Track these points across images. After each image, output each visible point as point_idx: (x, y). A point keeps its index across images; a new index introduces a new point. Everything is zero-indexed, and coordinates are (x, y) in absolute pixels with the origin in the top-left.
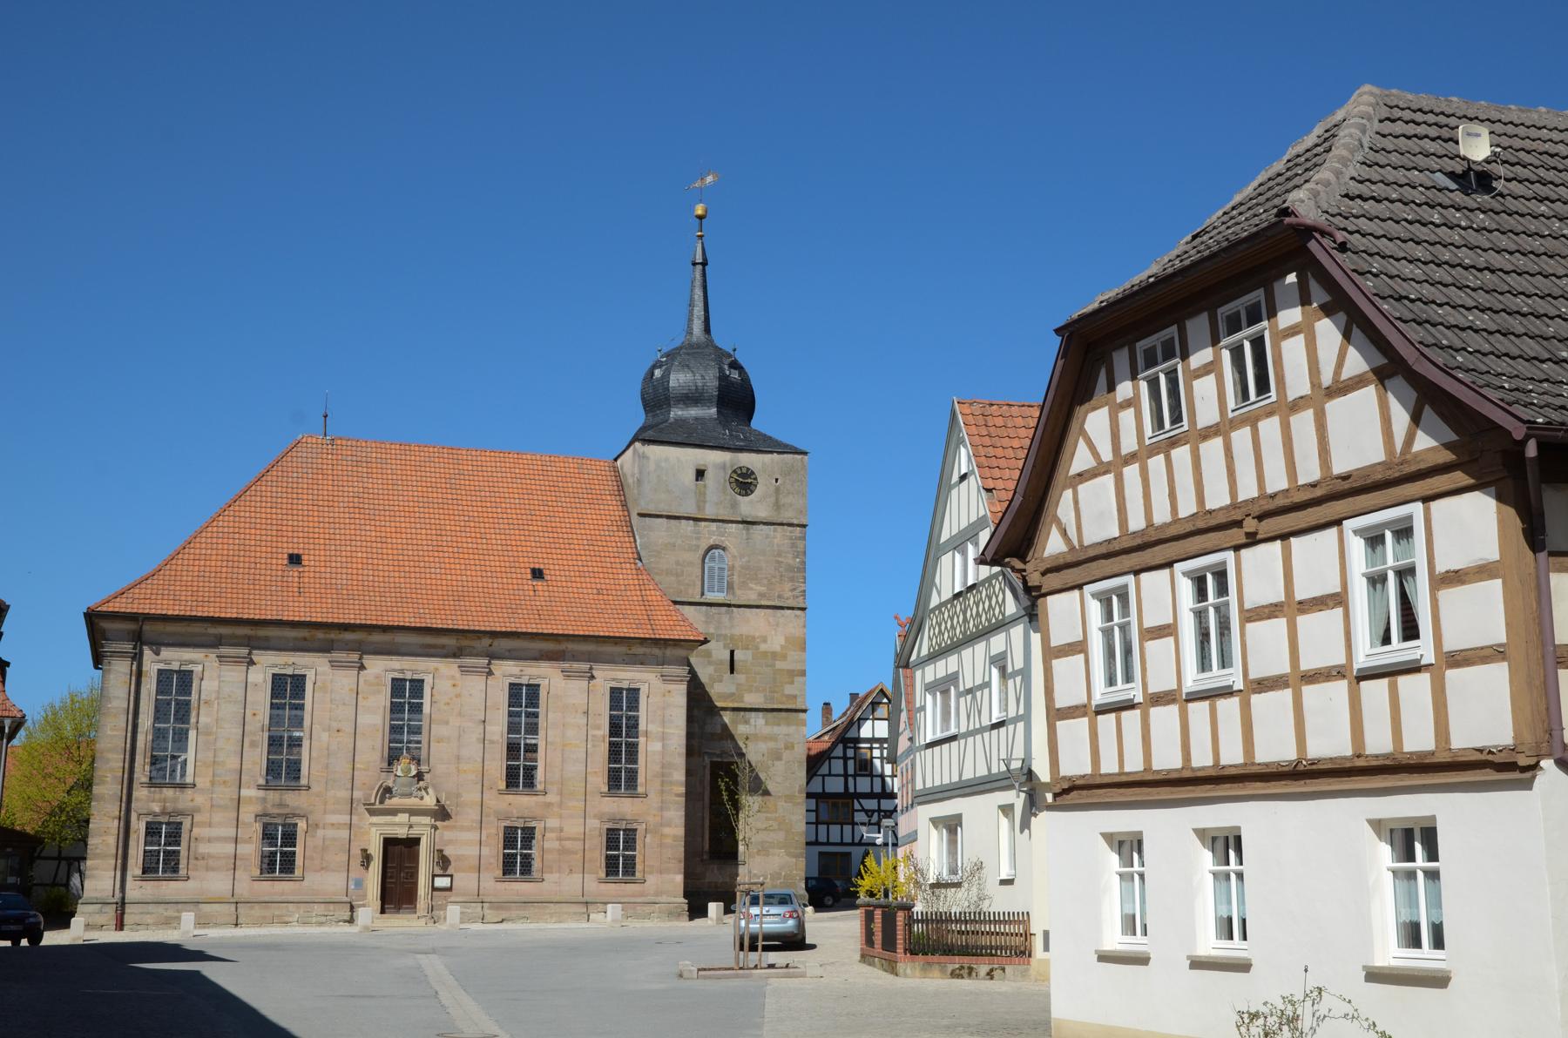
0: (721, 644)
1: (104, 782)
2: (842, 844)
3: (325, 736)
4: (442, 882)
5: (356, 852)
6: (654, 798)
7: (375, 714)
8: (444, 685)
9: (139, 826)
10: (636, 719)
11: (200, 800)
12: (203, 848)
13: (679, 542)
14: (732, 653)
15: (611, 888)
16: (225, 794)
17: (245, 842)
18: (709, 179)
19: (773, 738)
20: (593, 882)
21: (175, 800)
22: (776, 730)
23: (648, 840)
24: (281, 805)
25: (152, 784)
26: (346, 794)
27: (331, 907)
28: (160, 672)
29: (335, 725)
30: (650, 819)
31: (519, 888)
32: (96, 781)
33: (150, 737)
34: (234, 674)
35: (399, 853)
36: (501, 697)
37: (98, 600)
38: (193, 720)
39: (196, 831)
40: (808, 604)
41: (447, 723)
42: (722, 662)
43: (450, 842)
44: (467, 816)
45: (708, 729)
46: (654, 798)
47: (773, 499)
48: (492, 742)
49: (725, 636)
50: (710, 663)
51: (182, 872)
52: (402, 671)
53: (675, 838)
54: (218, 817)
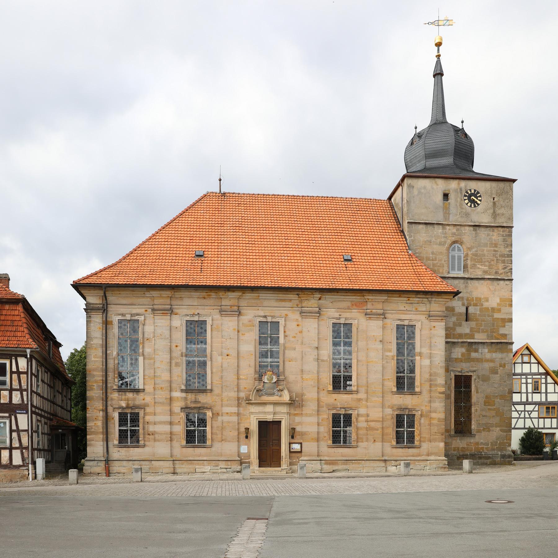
0: (460, 303)
1: (92, 389)
2: (551, 428)
3: (219, 358)
4: (296, 447)
5: (243, 430)
6: (425, 394)
7: (249, 345)
8: (292, 325)
11: (149, 399)
12: (151, 428)
13: (433, 240)
14: (467, 309)
15: (400, 452)
16: (162, 395)
19: (492, 361)
20: (389, 448)
21: (134, 399)
22: (494, 355)
23: (422, 421)
24: (196, 402)
25: (120, 390)
26: (233, 394)
27: (229, 463)
29: (225, 352)
30: (423, 408)
31: (341, 452)
32: (88, 388)
34: (162, 322)
35: (268, 431)
36: (328, 333)
37: (80, 277)
38: (141, 351)
39: (147, 418)
40: (513, 277)
41: (295, 349)
42: (460, 314)
43: (300, 423)
44: (311, 407)
46: (425, 395)
47: (492, 211)
48: (323, 361)
50: (453, 315)
51: (141, 443)
53: (439, 420)
54: (159, 409)
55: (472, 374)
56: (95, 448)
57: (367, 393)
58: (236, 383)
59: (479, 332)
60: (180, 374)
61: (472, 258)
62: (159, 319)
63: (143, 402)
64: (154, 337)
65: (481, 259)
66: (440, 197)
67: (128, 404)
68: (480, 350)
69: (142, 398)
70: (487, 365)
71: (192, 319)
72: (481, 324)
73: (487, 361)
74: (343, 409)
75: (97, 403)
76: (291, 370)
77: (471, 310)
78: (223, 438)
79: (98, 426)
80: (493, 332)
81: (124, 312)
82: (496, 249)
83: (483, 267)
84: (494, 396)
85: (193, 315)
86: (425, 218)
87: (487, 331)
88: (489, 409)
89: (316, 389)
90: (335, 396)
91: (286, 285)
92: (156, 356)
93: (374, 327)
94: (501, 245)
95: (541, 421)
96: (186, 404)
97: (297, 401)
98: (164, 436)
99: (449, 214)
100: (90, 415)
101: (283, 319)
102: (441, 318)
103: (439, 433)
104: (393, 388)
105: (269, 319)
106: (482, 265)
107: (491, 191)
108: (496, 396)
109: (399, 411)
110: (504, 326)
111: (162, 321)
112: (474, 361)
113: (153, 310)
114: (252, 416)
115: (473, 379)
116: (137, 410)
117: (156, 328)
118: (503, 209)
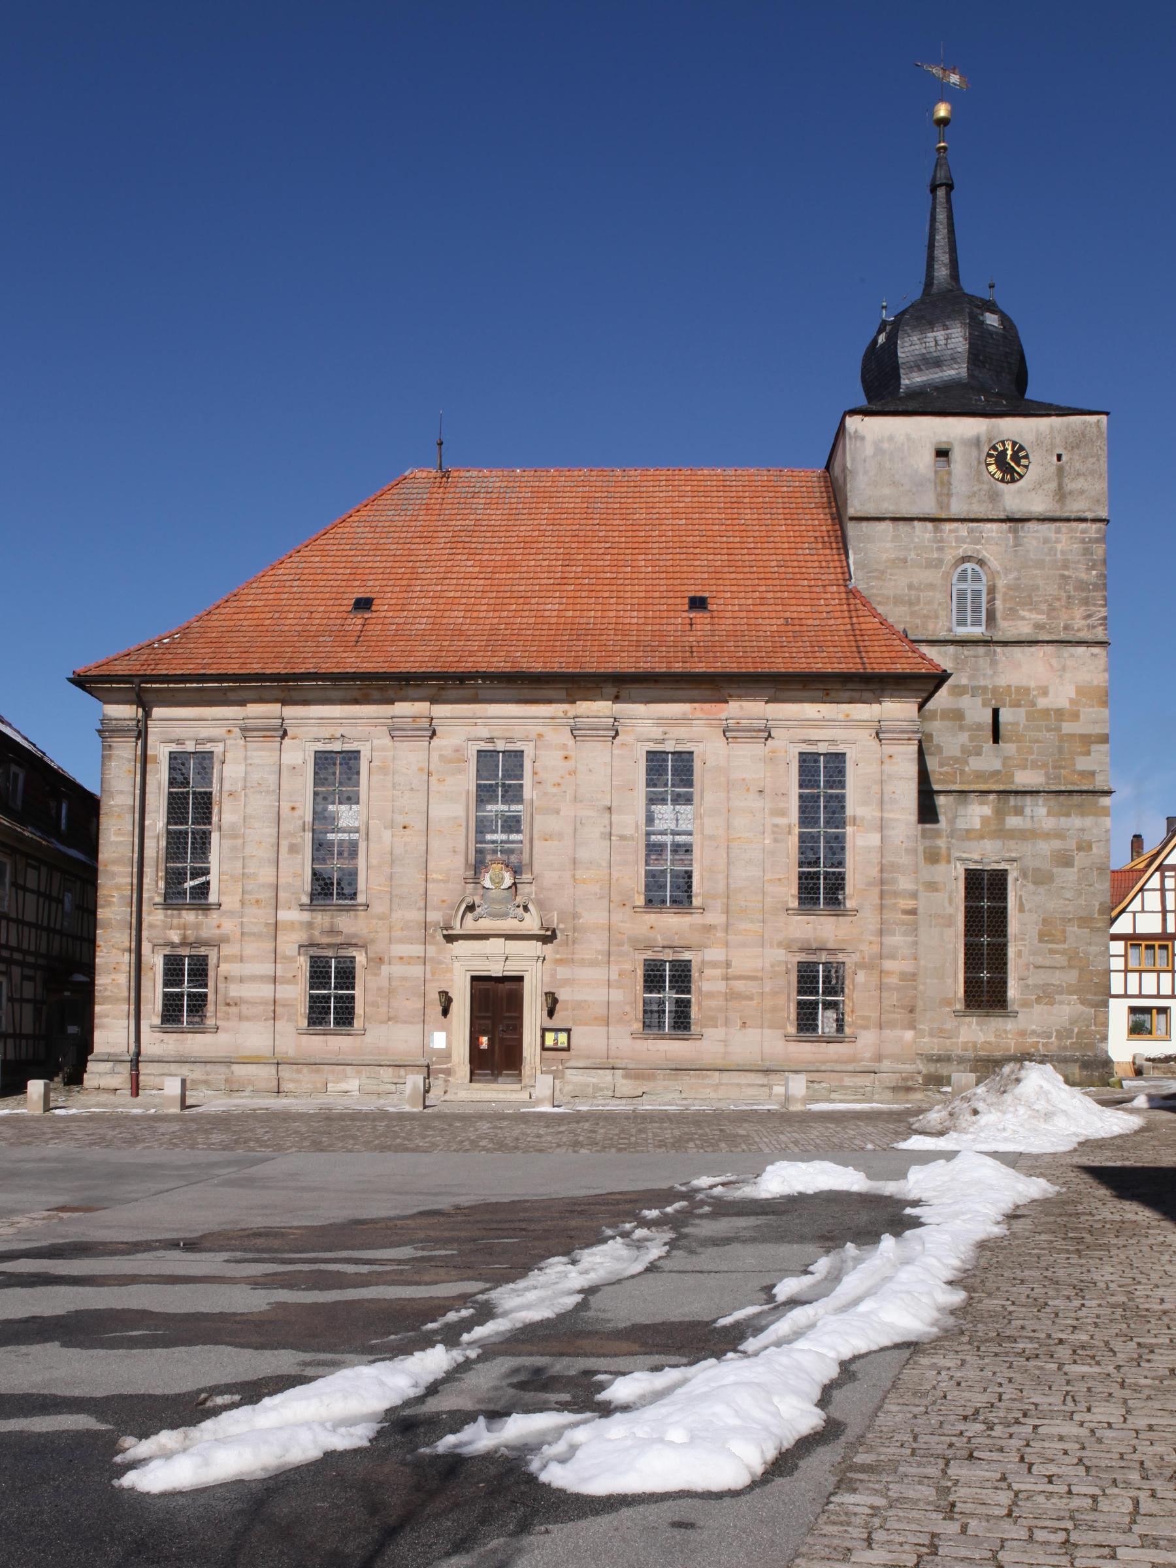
0: (979, 701)
1: (109, 904)
2: (1158, 996)
3: (387, 834)
9: (155, 962)
10: (841, 799)
11: (229, 926)
12: (235, 991)
14: (996, 713)
16: (257, 917)
17: (288, 982)
18: (954, 79)
19: (1059, 835)
21: (198, 926)
22: (1064, 822)
24: (332, 932)
28: (173, 756)
29: (400, 819)
31: (336, 1044)
32: (100, 902)
33: (163, 843)
34: (262, 754)
38: (215, 819)
39: (224, 967)
42: (979, 727)
43: (566, 982)
45: (961, 824)
46: (868, 919)
47: (1053, 485)
48: (622, 838)
49: (984, 689)
50: (961, 728)
51: (210, 1022)
52: (491, 740)
54: (250, 948)
55: (1007, 867)
56: (111, 1032)
57: (727, 913)
58: (422, 891)
59: (1025, 768)
60: (298, 872)
61: (1005, 594)
62: (256, 750)
63: (217, 931)
64: (245, 788)
65: (1030, 597)
66: (928, 456)
67: (184, 937)
68: (1028, 811)
69: (215, 923)
70: (1045, 848)
71: (329, 747)
72: (1031, 748)
73: (1047, 836)
74: (667, 950)
75: (118, 935)
76: (547, 857)
77: (1005, 716)
78: (391, 1015)
79: (118, 985)
80: (1060, 767)
81: (182, 736)
82: (1066, 573)
83: (1033, 616)
84: (1063, 919)
85: (332, 739)
86: (892, 508)
87: (1044, 765)
88: (1052, 952)
89: (605, 902)
90: (652, 918)
91: (538, 667)
92: (248, 831)
93: (746, 759)
94: (1078, 562)
95: (1133, 978)
96: (311, 937)
97: (563, 931)
98: (261, 1008)
99: (949, 495)
100: (103, 960)
101: (532, 744)
102: (906, 736)
103: (902, 1007)
104: (790, 899)
105: (501, 746)
106: (1030, 610)
107: (1053, 438)
108: (1070, 920)
109: (803, 955)
110: (1088, 753)
111: (263, 753)
112: (1012, 838)
113: (244, 729)
114: (457, 964)
115: (1010, 879)
116: (203, 949)
117: (249, 768)
118: (1081, 479)
